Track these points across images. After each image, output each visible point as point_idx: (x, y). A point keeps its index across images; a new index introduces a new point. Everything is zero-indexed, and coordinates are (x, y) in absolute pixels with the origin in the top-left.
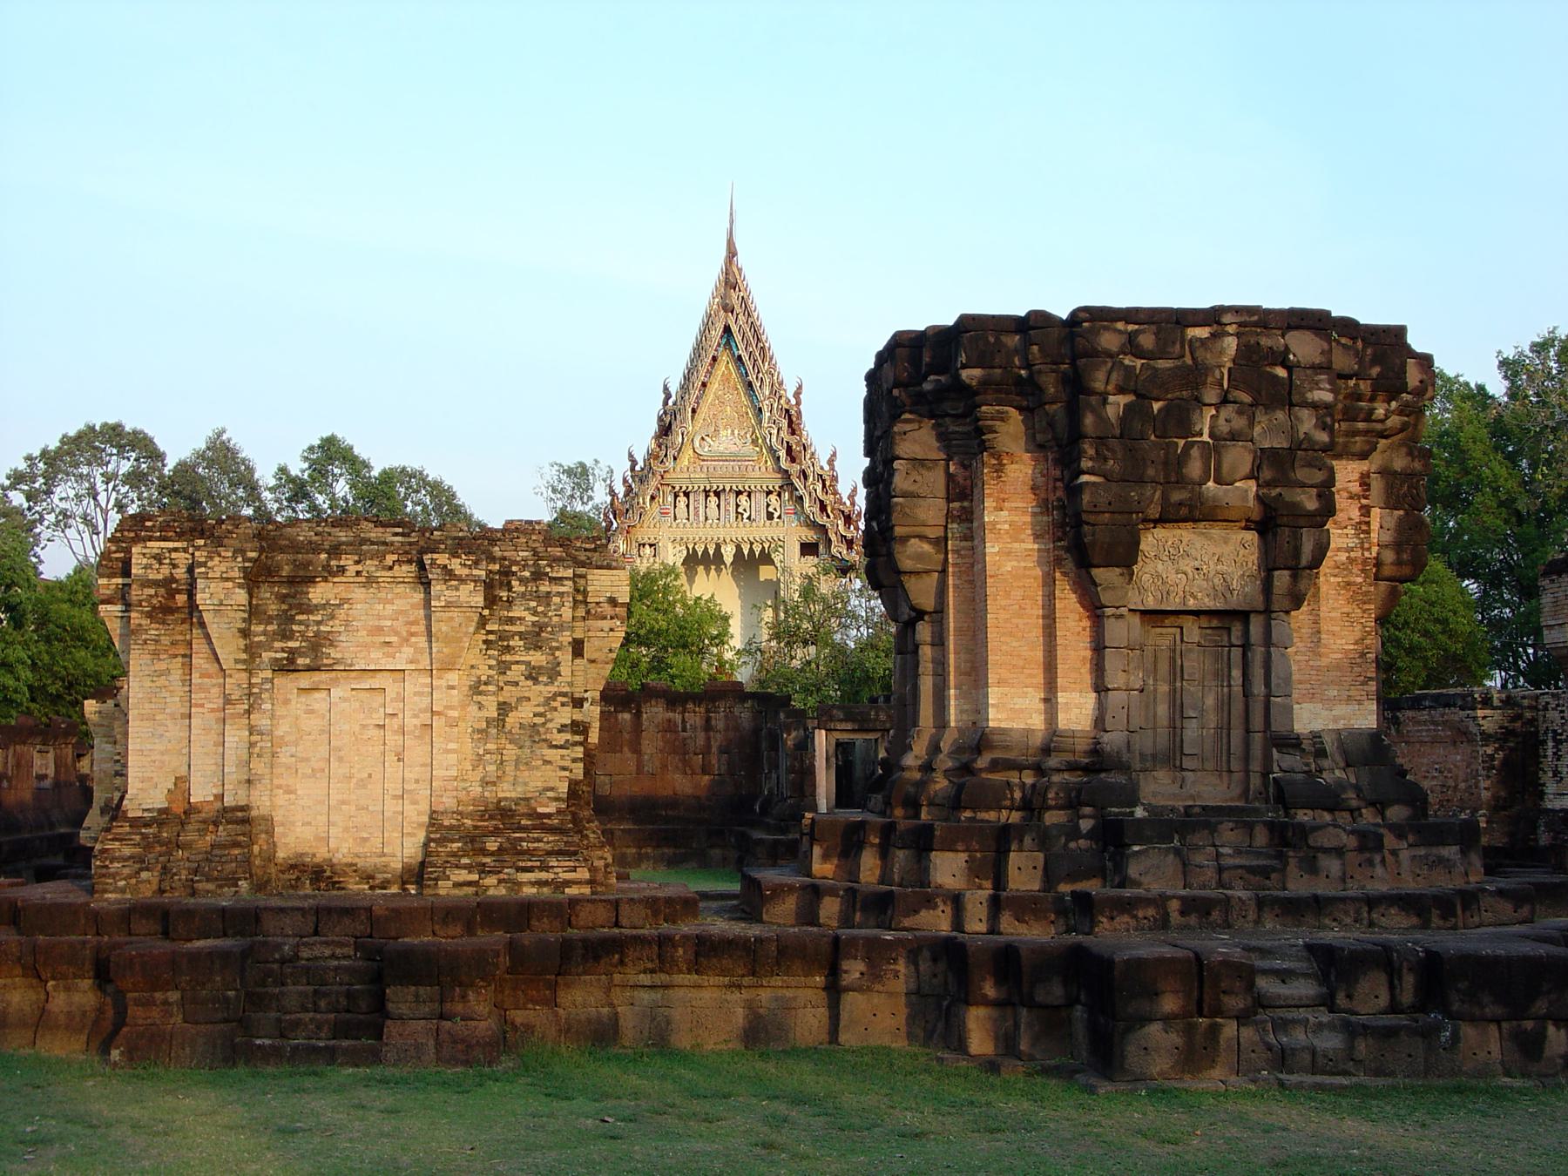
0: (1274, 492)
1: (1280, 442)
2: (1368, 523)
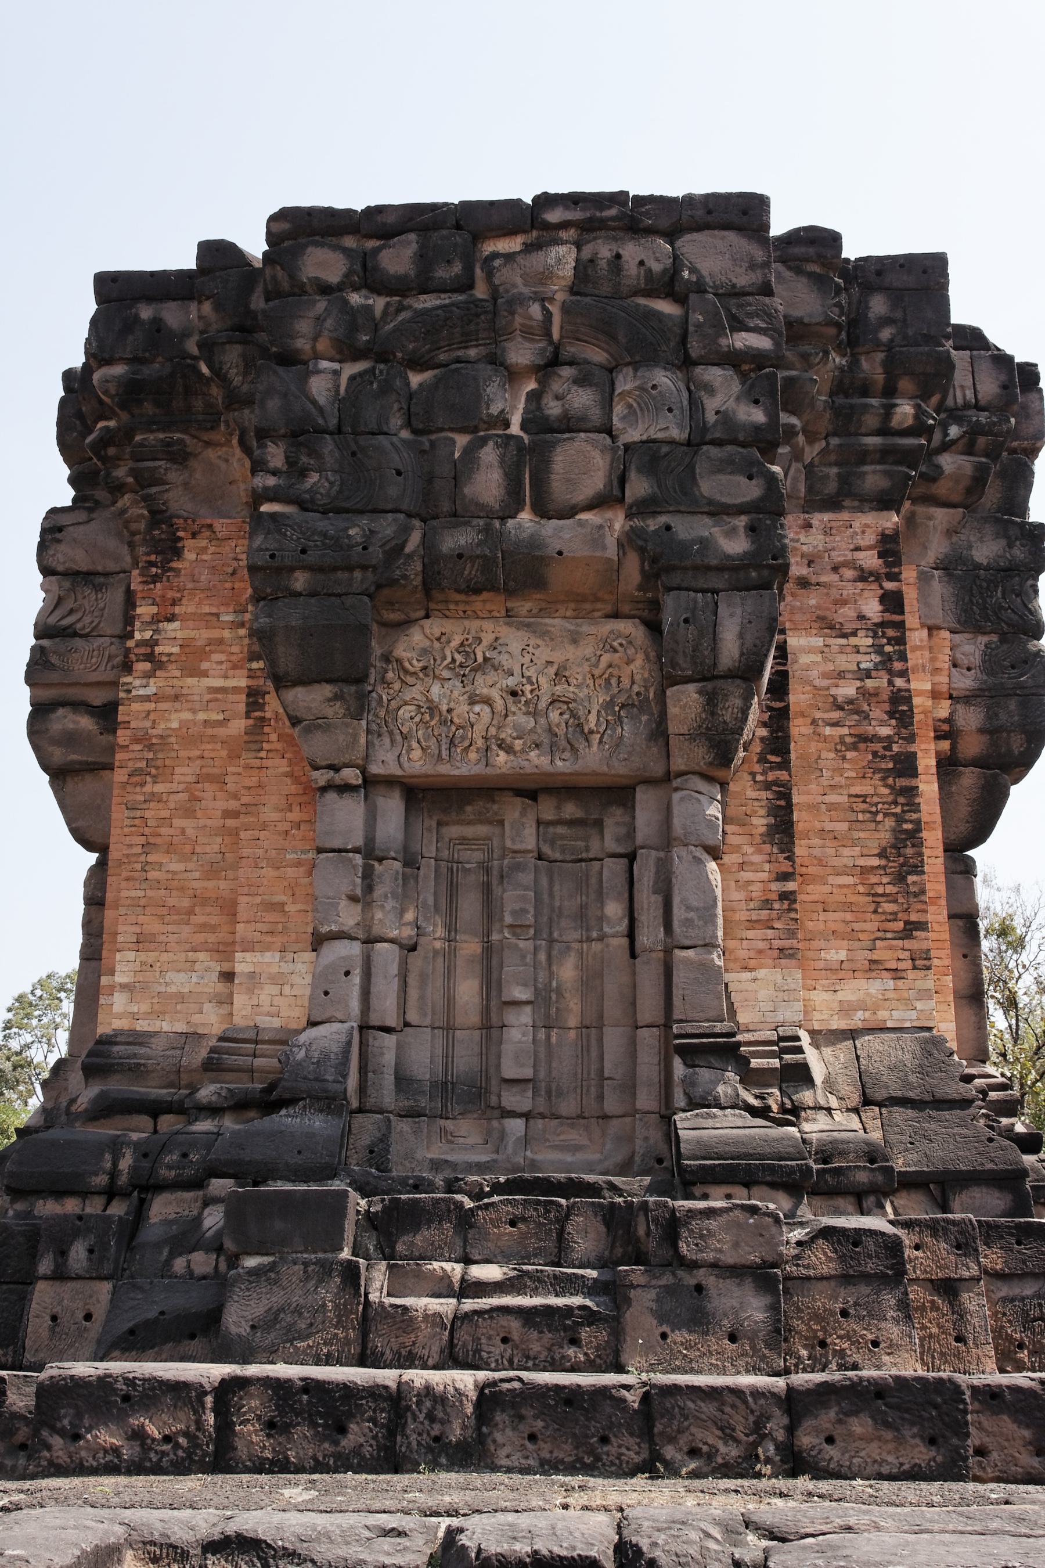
0: (653, 524)
1: (672, 428)
2: (901, 625)
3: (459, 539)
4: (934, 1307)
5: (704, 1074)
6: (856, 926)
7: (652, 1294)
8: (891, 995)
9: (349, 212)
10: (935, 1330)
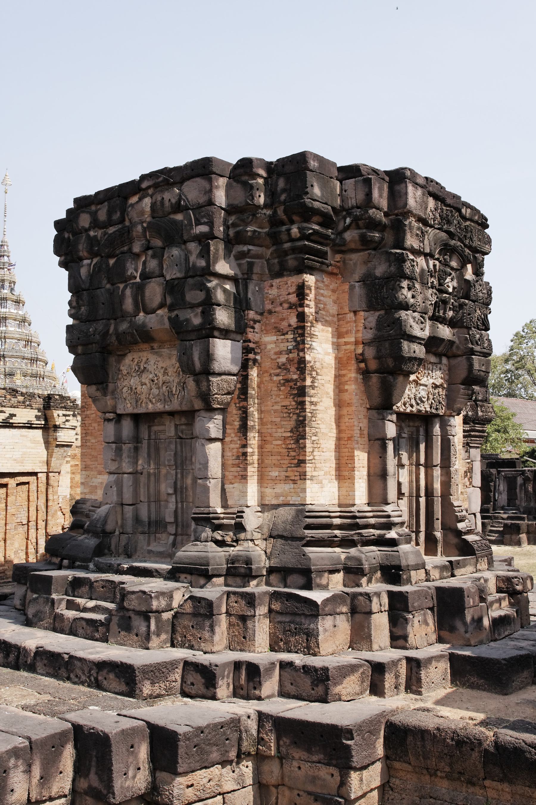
3: (124, 326)
4: (238, 625)
5: (200, 528)
6: (282, 462)
7: (117, 618)
8: (292, 490)
9: (91, 196)
10: (237, 633)
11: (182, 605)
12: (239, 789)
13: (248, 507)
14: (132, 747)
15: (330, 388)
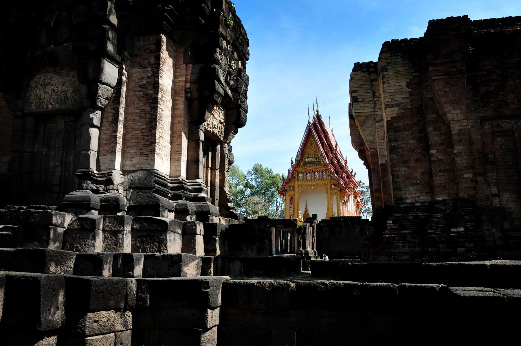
8: (145, 161)
11: (71, 224)
12: (124, 331)
13: (115, 170)
14: (54, 291)
15: (170, 104)
